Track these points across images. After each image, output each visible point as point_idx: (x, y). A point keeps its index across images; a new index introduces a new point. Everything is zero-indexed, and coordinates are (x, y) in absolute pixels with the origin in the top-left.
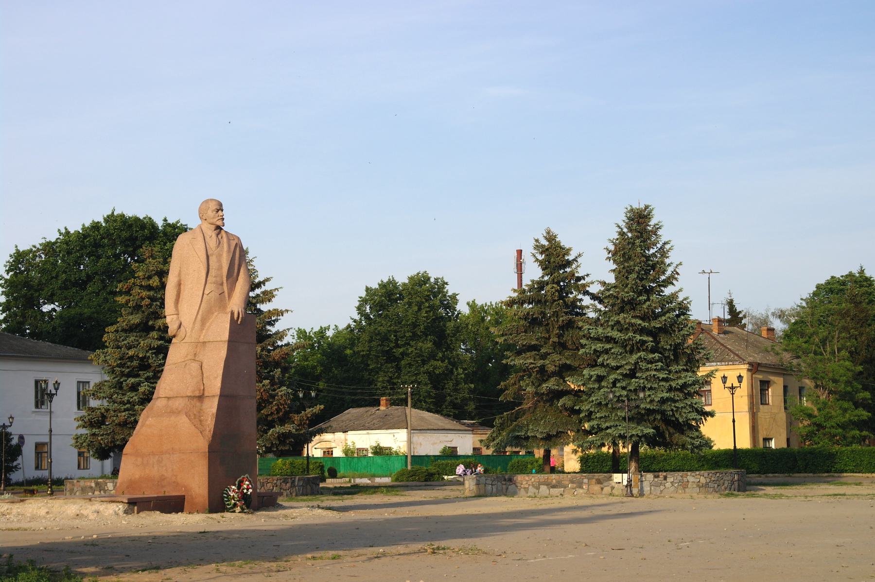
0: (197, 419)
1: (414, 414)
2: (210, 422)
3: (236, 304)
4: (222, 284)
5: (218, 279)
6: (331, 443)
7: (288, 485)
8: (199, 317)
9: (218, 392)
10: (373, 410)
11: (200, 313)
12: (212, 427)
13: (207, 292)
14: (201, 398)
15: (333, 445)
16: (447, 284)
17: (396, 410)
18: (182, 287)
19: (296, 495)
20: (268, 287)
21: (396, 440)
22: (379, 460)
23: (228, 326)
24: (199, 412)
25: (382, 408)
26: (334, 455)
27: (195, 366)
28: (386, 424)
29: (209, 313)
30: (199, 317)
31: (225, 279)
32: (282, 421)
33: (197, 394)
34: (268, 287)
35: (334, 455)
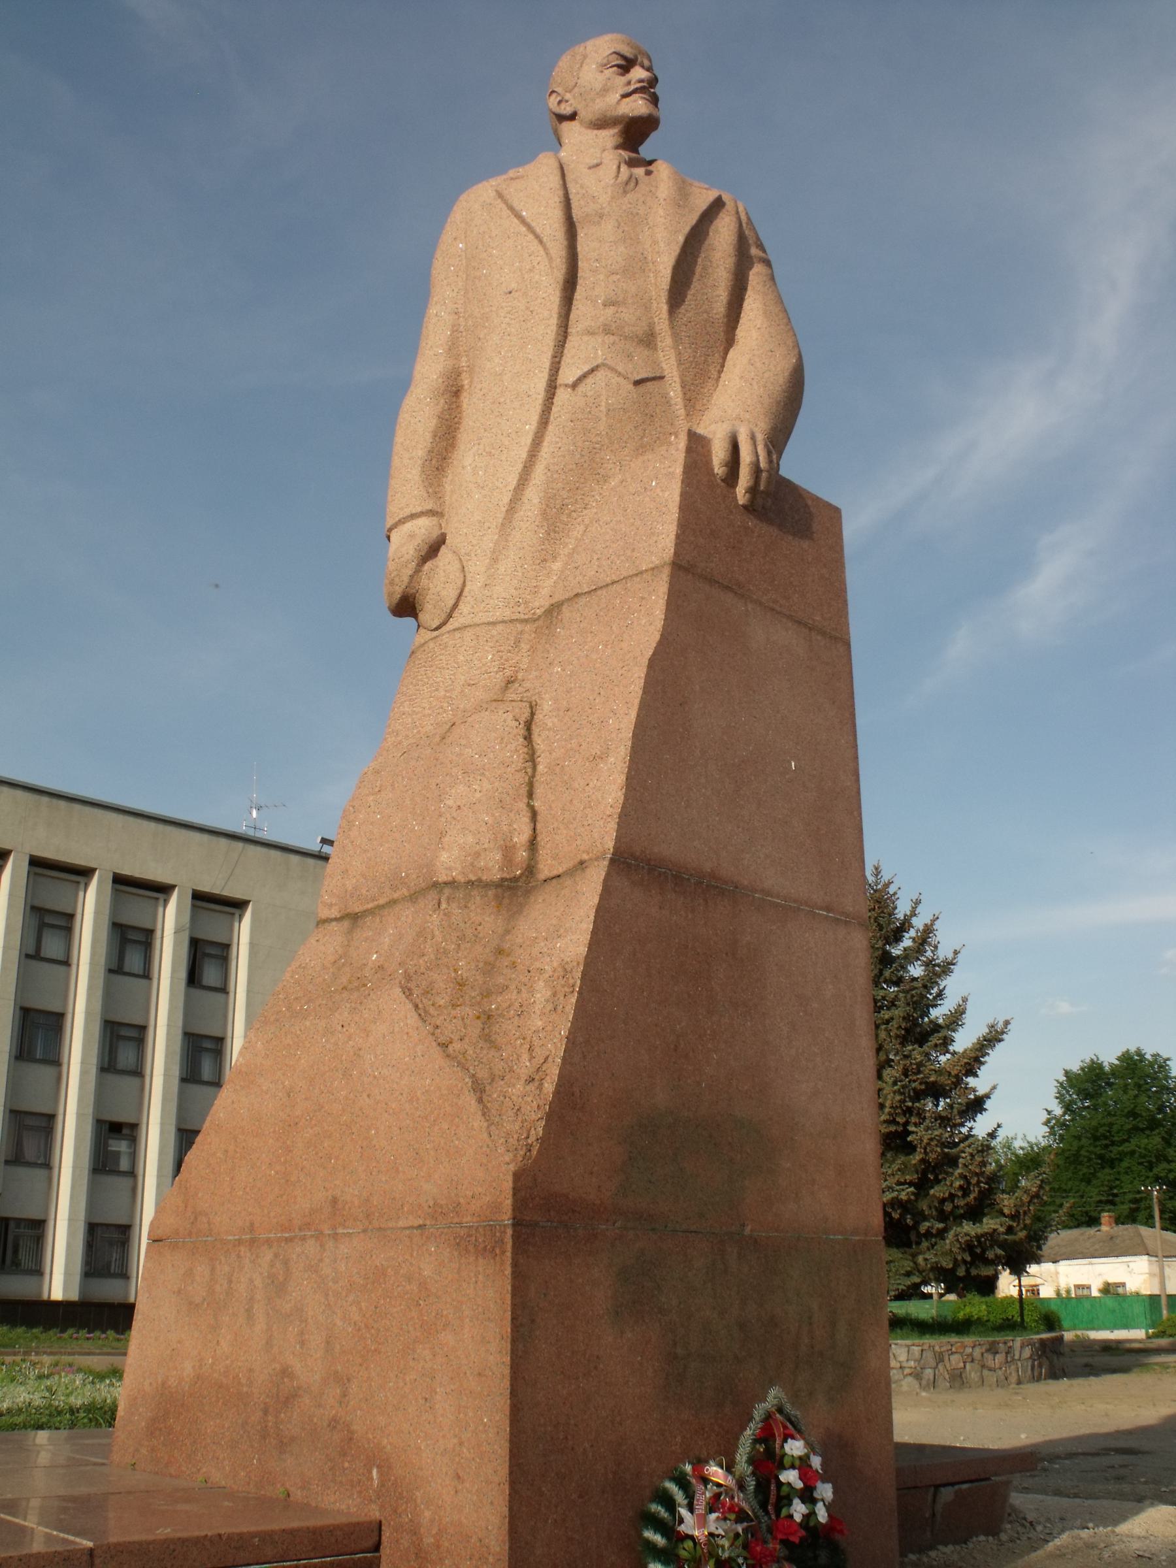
0: (468, 1008)
1: (1153, 1234)
2: (542, 1023)
3: (734, 408)
4: (648, 340)
5: (628, 315)
6: (1056, 1277)
7: (1000, 1358)
8: (533, 496)
9: (606, 837)
10: (1091, 1231)
11: (539, 474)
12: (554, 1047)
13: (568, 374)
14: (516, 887)
15: (1039, 1281)
16: (1168, 1059)
17: (1126, 1231)
18: (465, 399)
19: (1019, 1383)
20: (918, 923)
21: (1135, 1274)
22: (1110, 1302)
23: (672, 494)
24: (489, 969)
25: (1104, 1228)
26: (1042, 1295)
27: (506, 721)
28: (1112, 1250)
29: (587, 469)
30: (533, 496)
31: (661, 307)
32: (975, 1214)
33: (492, 866)
34: (918, 923)
35: (1042, 1295)
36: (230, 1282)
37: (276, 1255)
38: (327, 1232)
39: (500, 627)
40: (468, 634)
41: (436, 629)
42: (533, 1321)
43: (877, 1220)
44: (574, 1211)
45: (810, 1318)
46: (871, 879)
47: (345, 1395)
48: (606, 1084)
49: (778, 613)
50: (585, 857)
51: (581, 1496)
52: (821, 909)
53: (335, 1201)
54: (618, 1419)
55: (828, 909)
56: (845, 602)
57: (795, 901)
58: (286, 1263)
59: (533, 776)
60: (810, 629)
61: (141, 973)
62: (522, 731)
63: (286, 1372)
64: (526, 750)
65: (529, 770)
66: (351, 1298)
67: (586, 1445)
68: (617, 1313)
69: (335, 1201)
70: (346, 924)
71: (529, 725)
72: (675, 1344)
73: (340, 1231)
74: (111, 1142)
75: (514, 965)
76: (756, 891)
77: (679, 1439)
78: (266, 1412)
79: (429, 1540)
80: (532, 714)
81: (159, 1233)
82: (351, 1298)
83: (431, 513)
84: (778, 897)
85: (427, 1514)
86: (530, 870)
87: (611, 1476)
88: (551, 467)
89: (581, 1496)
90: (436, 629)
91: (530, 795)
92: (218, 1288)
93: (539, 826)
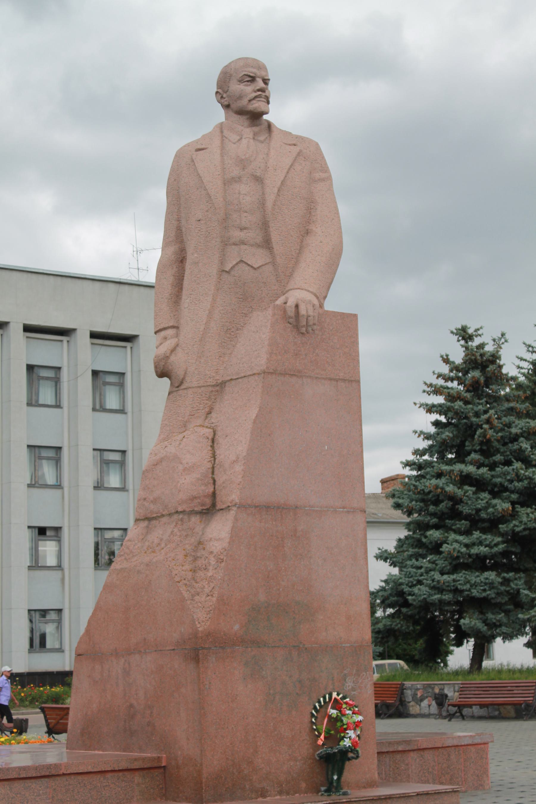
36: (109, 671)
37: (125, 661)
38: (143, 651)
39: (202, 389)
40: (190, 391)
41: (178, 387)
42: (210, 683)
43: (368, 635)
44: (225, 643)
45: (333, 678)
46: (6, 732)
47: (152, 713)
48: (238, 594)
49: (319, 378)
50: (230, 505)
51: (231, 744)
52: (340, 508)
53: (145, 639)
54: (246, 717)
55: (344, 508)
56: (358, 361)
57: (326, 507)
58: (129, 664)
59: (214, 464)
60: (337, 381)
61: (53, 403)
62: (210, 443)
63: (131, 706)
64: (211, 452)
65: (213, 462)
66: (152, 676)
67: (233, 726)
68: (244, 679)
69: (145, 639)
70: (146, 523)
71: (213, 441)
72: (270, 689)
73: (147, 651)
74: (40, 543)
75: (204, 549)
76: (306, 507)
77: (272, 724)
78: (125, 721)
79: (180, 762)
80: (215, 434)
81: (80, 652)
82: (152, 676)
83: (173, 327)
84: (317, 507)
85: (180, 753)
86: (214, 505)
87: (243, 737)
88: (222, 312)
89: (231, 744)
90: (178, 387)
91: (213, 473)
92: (105, 675)
93: (216, 487)
